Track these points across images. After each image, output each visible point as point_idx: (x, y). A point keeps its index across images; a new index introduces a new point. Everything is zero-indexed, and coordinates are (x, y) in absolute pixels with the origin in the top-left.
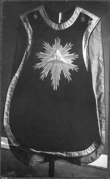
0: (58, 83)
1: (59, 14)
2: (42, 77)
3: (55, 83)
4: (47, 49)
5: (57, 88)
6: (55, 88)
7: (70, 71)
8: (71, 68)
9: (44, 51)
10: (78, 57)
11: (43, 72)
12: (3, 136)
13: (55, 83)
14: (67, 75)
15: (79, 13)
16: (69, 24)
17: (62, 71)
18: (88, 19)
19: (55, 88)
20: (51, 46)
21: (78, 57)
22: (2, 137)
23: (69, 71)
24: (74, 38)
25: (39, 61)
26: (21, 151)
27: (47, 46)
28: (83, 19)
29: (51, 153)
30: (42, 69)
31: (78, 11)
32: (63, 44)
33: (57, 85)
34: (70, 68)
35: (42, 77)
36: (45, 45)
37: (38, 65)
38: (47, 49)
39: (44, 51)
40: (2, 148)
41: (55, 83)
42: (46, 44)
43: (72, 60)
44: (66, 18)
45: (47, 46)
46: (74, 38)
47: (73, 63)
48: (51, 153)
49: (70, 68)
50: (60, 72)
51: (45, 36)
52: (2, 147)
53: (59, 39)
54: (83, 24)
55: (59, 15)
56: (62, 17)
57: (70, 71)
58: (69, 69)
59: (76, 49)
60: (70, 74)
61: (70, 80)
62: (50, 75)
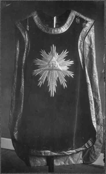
0: (55, 89)
1: (54, 18)
2: (40, 84)
3: (53, 89)
4: (44, 56)
5: (54, 95)
6: (53, 94)
7: (66, 77)
8: (66, 75)
9: (41, 58)
10: (73, 63)
11: (40, 78)
12: (2, 137)
13: (53, 89)
14: (64, 83)
15: (75, 16)
16: (64, 29)
17: (58, 78)
18: (83, 21)
19: (53, 94)
20: (48, 54)
21: (73, 63)
22: (2, 138)
23: (65, 78)
24: (68, 44)
25: (37, 67)
26: (26, 147)
27: (44, 53)
28: (78, 21)
29: (22, 107)
30: (39, 76)
31: (73, 14)
32: (59, 52)
33: (56, 86)
34: (66, 75)
35: (40, 84)
36: (42, 52)
37: (65, 53)
38: (44, 56)
39: (41, 58)
40: (2, 149)
41: (52, 91)
42: (42, 50)
43: (68, 67)
44: (60, 24)
45: (44, 53)
46: (68, 44)
47: (68, 70)
48: (22, 107)
49: (66, 75)
50: (56, 78)
51: (42, 43)
52: (2, 147)
53: (54, 47)
54: (77, 28)
55: (54, 19)
56: (57, 20)
57: (66, 77)
58: (65, 76)
59: (73, 55)
60: (65, 81)
61: (65, 87)
62: (46, 82)
